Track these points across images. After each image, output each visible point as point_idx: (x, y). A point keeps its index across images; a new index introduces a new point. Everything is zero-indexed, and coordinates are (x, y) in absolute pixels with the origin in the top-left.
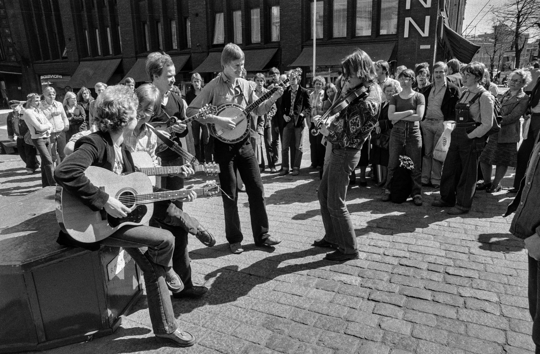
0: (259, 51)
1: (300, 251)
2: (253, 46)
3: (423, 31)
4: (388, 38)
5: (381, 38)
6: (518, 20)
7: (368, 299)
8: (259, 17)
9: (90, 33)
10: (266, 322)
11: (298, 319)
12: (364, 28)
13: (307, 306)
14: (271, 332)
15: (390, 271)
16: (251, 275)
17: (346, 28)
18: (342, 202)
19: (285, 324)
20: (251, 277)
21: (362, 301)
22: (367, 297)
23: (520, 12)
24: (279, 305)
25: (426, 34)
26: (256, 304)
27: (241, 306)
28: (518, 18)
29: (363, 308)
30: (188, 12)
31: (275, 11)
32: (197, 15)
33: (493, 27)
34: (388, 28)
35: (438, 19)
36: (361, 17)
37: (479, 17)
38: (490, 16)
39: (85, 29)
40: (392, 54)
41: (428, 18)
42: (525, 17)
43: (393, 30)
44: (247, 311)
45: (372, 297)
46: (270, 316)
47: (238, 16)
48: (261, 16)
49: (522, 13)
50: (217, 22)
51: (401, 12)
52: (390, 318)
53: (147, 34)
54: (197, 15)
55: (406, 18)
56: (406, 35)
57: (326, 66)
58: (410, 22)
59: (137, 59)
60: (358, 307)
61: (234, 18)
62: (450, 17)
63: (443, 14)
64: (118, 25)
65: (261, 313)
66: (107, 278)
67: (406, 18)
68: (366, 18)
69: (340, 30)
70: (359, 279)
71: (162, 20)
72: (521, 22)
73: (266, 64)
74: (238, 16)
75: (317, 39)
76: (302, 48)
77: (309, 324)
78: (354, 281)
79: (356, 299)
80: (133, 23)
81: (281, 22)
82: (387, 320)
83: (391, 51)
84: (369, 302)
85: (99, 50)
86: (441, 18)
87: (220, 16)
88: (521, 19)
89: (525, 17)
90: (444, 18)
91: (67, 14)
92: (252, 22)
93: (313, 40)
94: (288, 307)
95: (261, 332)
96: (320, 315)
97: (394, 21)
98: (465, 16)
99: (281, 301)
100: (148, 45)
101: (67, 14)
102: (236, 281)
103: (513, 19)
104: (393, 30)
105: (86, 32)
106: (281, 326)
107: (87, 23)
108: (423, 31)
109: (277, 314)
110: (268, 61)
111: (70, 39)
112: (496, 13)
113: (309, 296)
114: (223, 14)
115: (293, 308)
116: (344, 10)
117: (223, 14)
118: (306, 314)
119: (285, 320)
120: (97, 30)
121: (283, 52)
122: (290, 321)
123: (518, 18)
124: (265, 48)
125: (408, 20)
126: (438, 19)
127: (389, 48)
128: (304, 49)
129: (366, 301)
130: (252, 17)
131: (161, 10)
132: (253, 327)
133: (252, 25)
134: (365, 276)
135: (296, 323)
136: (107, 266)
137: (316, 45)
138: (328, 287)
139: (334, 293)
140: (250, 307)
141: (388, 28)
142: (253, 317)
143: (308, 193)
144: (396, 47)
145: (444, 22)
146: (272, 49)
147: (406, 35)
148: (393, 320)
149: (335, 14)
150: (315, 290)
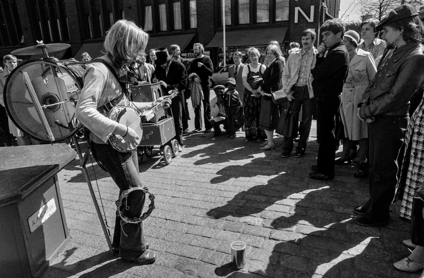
0: (180, 36)
1: (244, 164)
2: (175, 32)
3: (309, 18)
4: (282, 24)
5: (277, 23)
6: (380, 10)
7: (270, 239)
8: (180, 9)
9: (42, 23)
10: (179, 263)
11: (206, 260)
12: (263, 16)
13: (215, 247)
14: (181, 273)
15: (288, 212)
16: (167, 220)
17: (249, 16)
18: (156, 126)
19: (195, 264)
20: (167, 221)
21: (263, 240)
22: (268, 236)
23: (381, 4)
24: (191, 247)
25: (311, 20)
26: (170, 246)
27: (156, 249)
28: (380, 9)
29: (264, 247)
30: (122, 5)
31: (193, 5)
32: (130, 8)
33: (362, 16)
34: (282, 16)
35: (320, 8)
36: (261, 9)
37: (351, 9)
38: (360, 7)
39: (39, 21)
40: (286, 36)
41: (312, 7)
42: (385, 7)
43: (285, 18)
44: (161, 254)
45: (273, 236)
46: (182, 257)
47: (163, 8)
48: (181, 8)
49: (383, 4)
50: (146, 12)
51: (292, 3)
52: (289, 255)
53: (90, 24)
54: (130, 8)
55: (296, 8)
56: (296, 21)
57: (234, 47)
58: (299, 11)
59: (82, 44)
60: (260, 246)
61: (160, 10)
62: (330, 8)
63: (324, 4)
64: (66, 17)
65: (173, 255)
66: (27, 230)
67: (296, 8)
68: (264, 9)
69: (244, 18)
70: (262, 220)
71: (102, 12)
72: (382, 11)
73: (186, 46)
74: (163, 8)
75: (226, 26)
76: (215, 33)
77: (217, 264)
78: (256, 223)
79: (258, 238)
80: (78, 14)
81: (198, 14)
82: (287, 258)
83: (285, 34)
84: (270, 241)
85: (51, 37)
86: (322, 7)
87: (148, 9)
88: (382, 10)
89: (385, 7)
90: (325, 8)
91: (22, 8)
92: (174, 12)
93: (223, 26)
94: (198, 249)
95: (174, 273)
96: (227, 255)
97: (287, 12)
98: (341, 8)
99: (192, 243)
100: (91, 32)
101: (22, 8)
102: (153, 226)
103: (376, 9)
104: (285, 18)
105: (40, 22)
106: (191, 267)
107: (40, 15)
108: (309, 18)
109: (188, 256)
110: (188, 43)
111: (26, 29)
112: (364, 5)
113: (218, 237)
114: (150, 7)
115: (203, 249)
116: (246, 4)
117: (150, 7)
118: (214, 254)
119: (196, 261)
120: (49, 21)
121: (200, 37)
122: (199, 262)
123: (380, 9)
124: (185, 34)
125: (297, 9)
126: (320, 8)
127: (283, 32)
128: (216, 34)
129: (268, 240)
130: (174, 9)
131: (101, 5)
132: (165, 269)
133: (174, 15)
134: (266, 217)
135: (205, 263)
136: (28, 220)
137: (226, 30)
138: (234, 228)
139: (239, 234)
140: (165, 249)
141: (282, 16)
142: (166, 259)
143: (219, 147)
144: (288, 30)
145: (325, 11)
146: (191, 35)
147: (296, 21)
148: (292, 257)
149: (240, 7)
150: (223, 231)
